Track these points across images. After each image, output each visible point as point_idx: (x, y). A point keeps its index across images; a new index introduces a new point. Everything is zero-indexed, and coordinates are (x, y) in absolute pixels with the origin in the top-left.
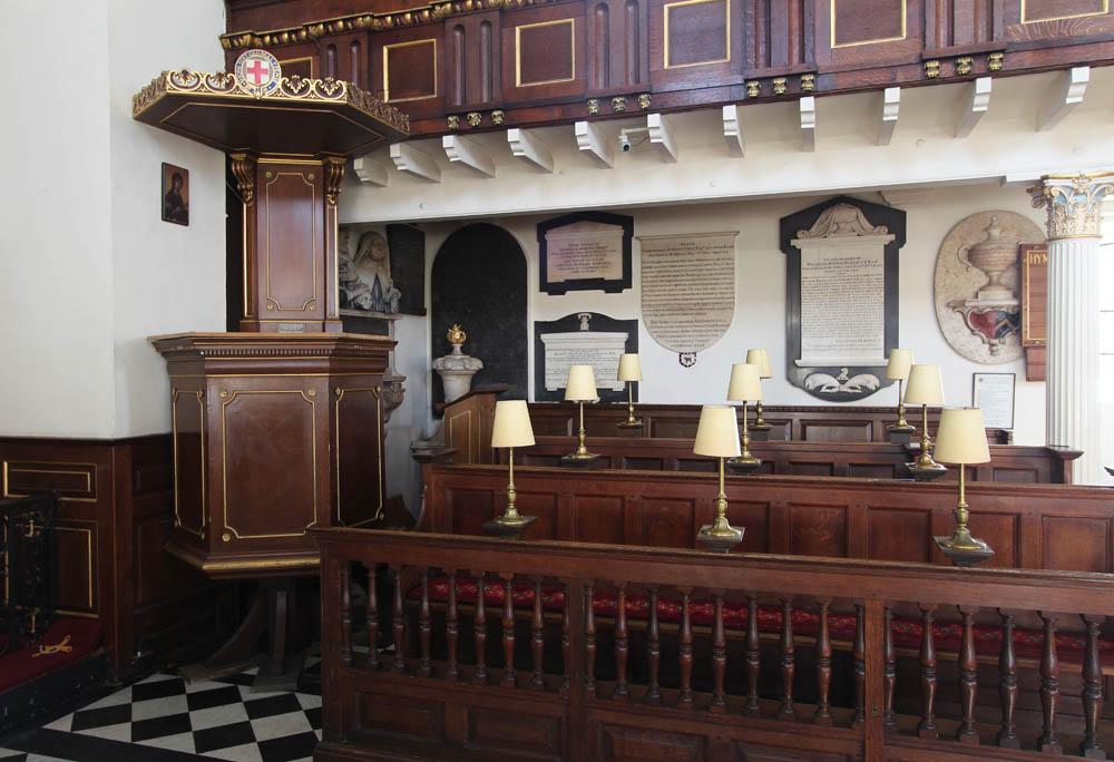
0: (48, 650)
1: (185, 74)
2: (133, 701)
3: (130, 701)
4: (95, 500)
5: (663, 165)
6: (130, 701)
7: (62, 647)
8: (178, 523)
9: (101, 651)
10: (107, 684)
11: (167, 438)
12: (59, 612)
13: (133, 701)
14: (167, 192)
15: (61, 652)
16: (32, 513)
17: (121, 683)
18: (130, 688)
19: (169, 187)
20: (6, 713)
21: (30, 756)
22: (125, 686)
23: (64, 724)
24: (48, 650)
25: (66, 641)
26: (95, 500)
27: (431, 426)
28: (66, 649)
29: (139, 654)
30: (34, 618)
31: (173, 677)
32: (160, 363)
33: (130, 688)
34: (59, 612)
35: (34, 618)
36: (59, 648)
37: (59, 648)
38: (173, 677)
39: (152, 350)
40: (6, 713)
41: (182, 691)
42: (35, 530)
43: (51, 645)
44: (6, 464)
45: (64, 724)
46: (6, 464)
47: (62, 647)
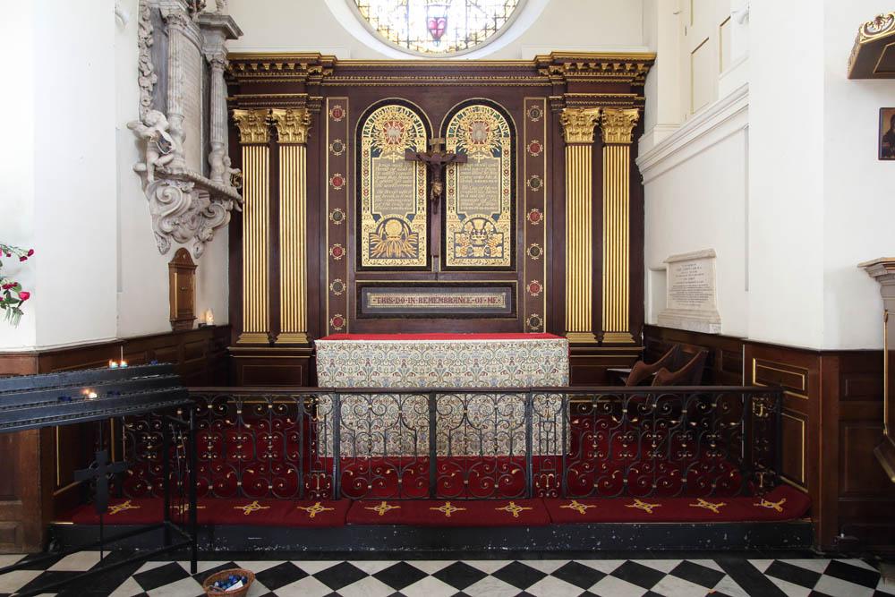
0: (766, 504)
1: (879, 19)
2: (826, 573)
3: (822, 572)
4: (807, 398)
5: (655, 65)
6: (822, 571)
7: (776, 506)
8: (886, 432)
9: (808, 520)
10: (812, 549)
11: (875, 356)
12: (783, 478)
13: (826, 573)
14: (884, 133)
15: (774, 508)
16: (762, 399)
17: (824, 553)
18: (828, 561)
19: (887, 128)
20: (725, 538)
21: (727, 577)
22: (826, 557)
23: (762, 565)
24: (766, 504)
25: (781, 502)
26: (807, 398)
27: (591, 339)
28: (778, 508)
29: (842, 535)
30: (762, 477)
31: (873, 569)
32: (874, 287)
33: (828, 561)
34: (783, 478)
35: (762, 477)
36: (774, 505)
37: (774, 505)
38: (873, 569)
39: (865, 276)
40: (725, 538)
41: (873, 585)
42: (765, 411)
43: (770, 501)
44: (754, 360)
45: (762, 565)
46: (754, 360)
47: (776, 506)
